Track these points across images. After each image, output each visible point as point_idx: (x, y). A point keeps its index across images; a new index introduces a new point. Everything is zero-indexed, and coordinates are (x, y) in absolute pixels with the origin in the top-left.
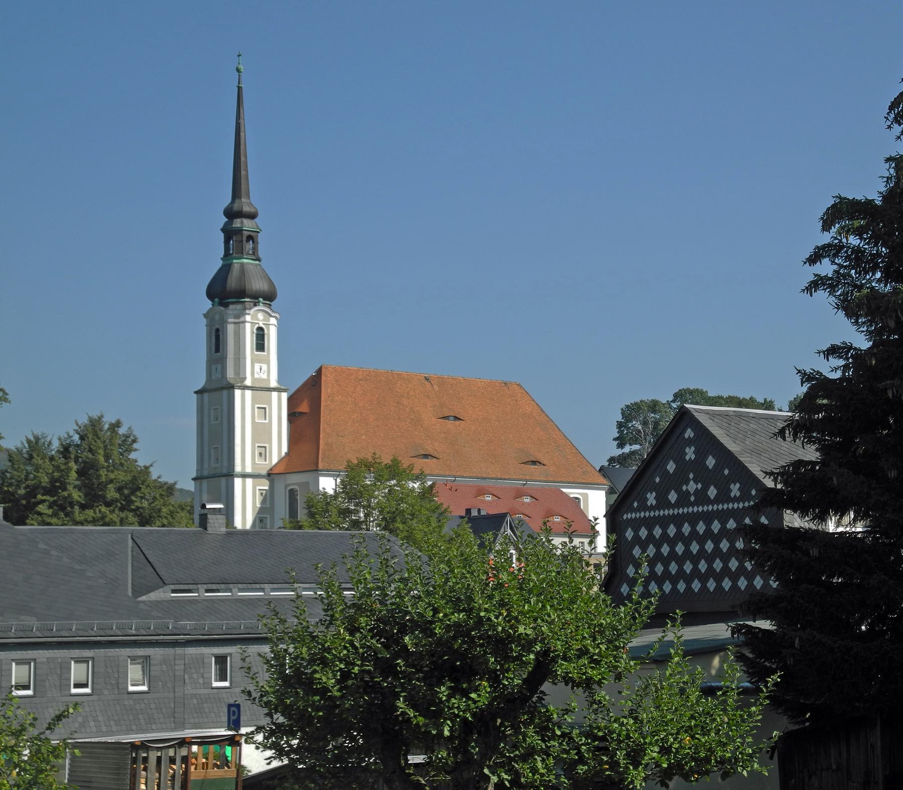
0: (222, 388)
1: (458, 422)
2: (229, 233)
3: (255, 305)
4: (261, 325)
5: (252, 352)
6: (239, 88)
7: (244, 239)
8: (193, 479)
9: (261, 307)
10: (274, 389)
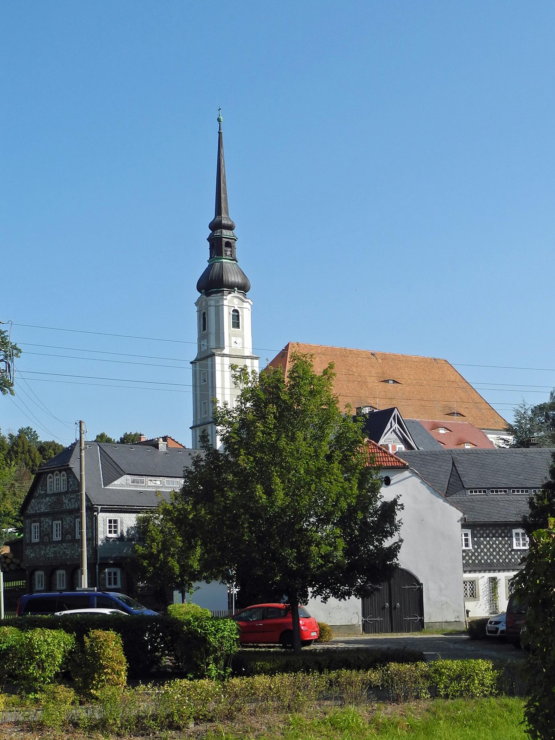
0: (208, 357)
1: (396, 385)
3: (230, 293)
4: (236, 308)
5: (229, 328)
6: (220, 133)
7: (224, 244)
8: (190, 428)
9: (236, 294)
10: (248, 357)
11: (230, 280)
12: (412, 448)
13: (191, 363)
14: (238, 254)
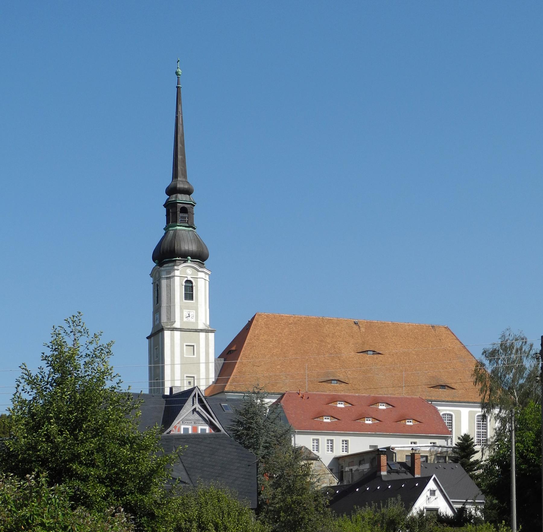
2: (170, 206)
4: (189, 279)
5: (181, 300)
7: (179, 210)
9: (189, 263)
10: (202, 331)
11: (183, 249)
12: (219, 430)
13: (148, 338)
14: (197, 220)
